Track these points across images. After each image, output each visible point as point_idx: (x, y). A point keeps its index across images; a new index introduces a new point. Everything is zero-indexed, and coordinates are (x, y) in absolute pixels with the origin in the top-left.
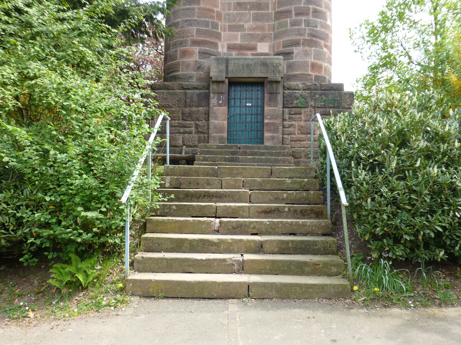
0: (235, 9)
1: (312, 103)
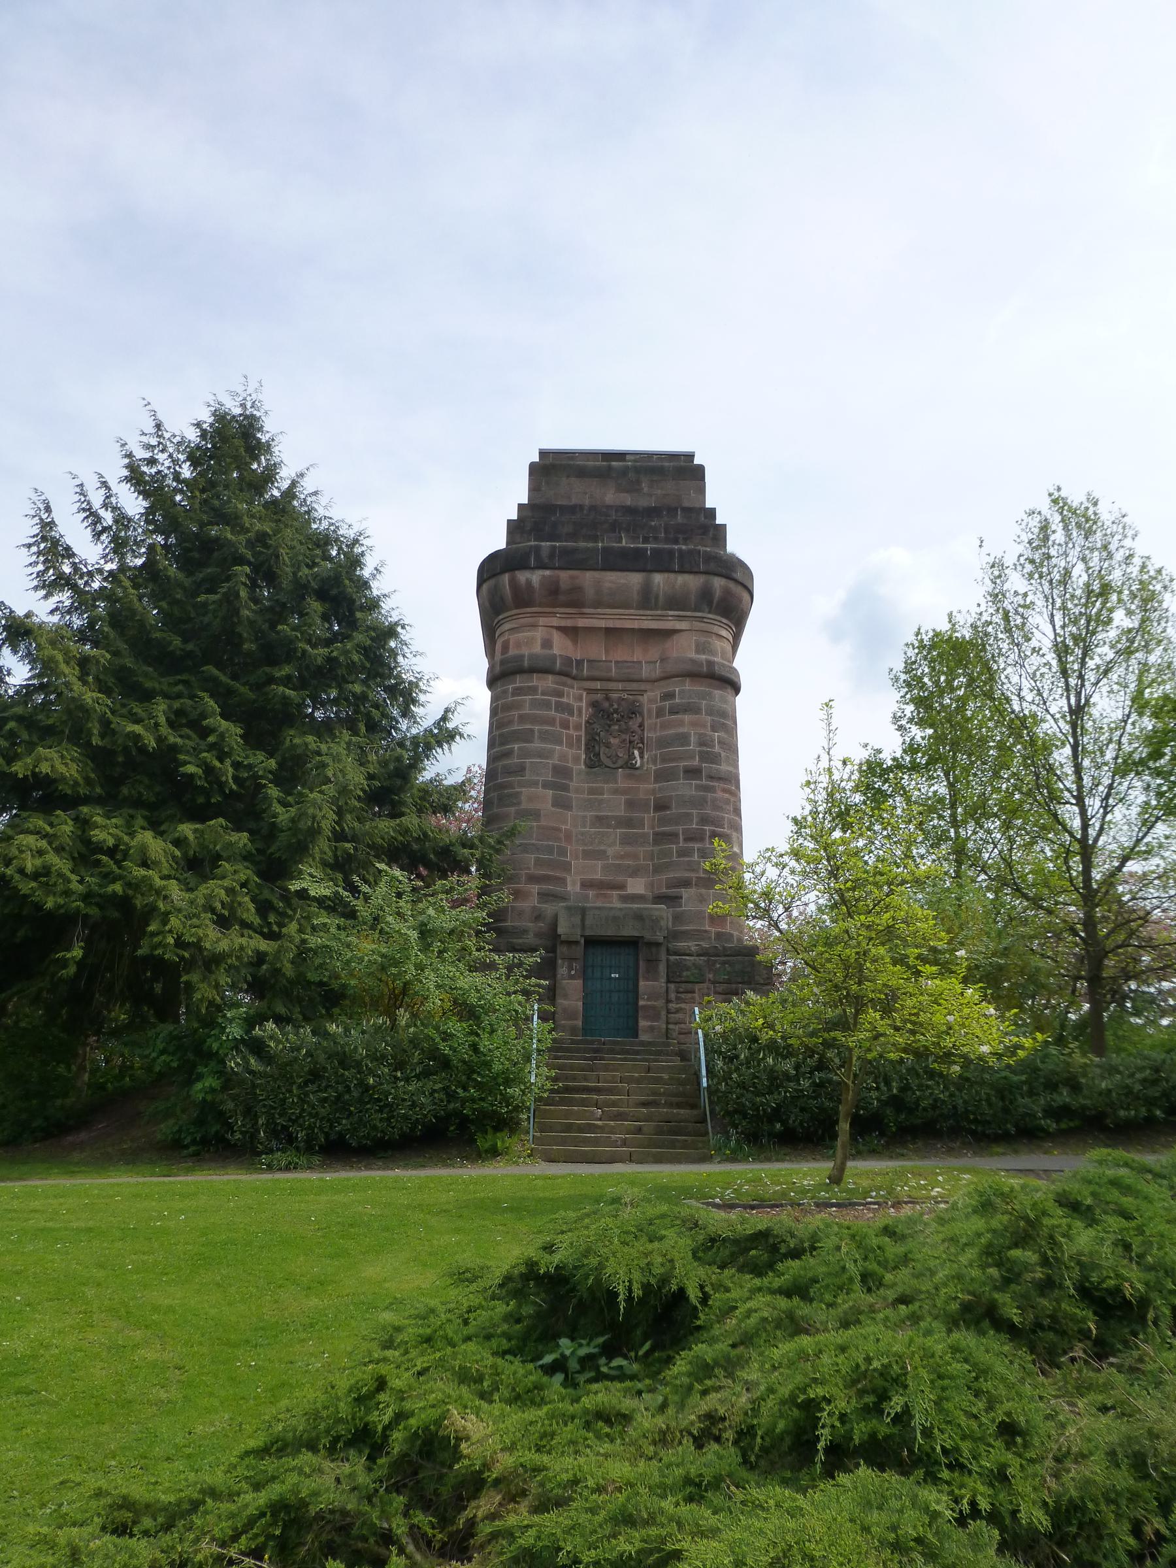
0: (593, 825)
1: (711, 976)
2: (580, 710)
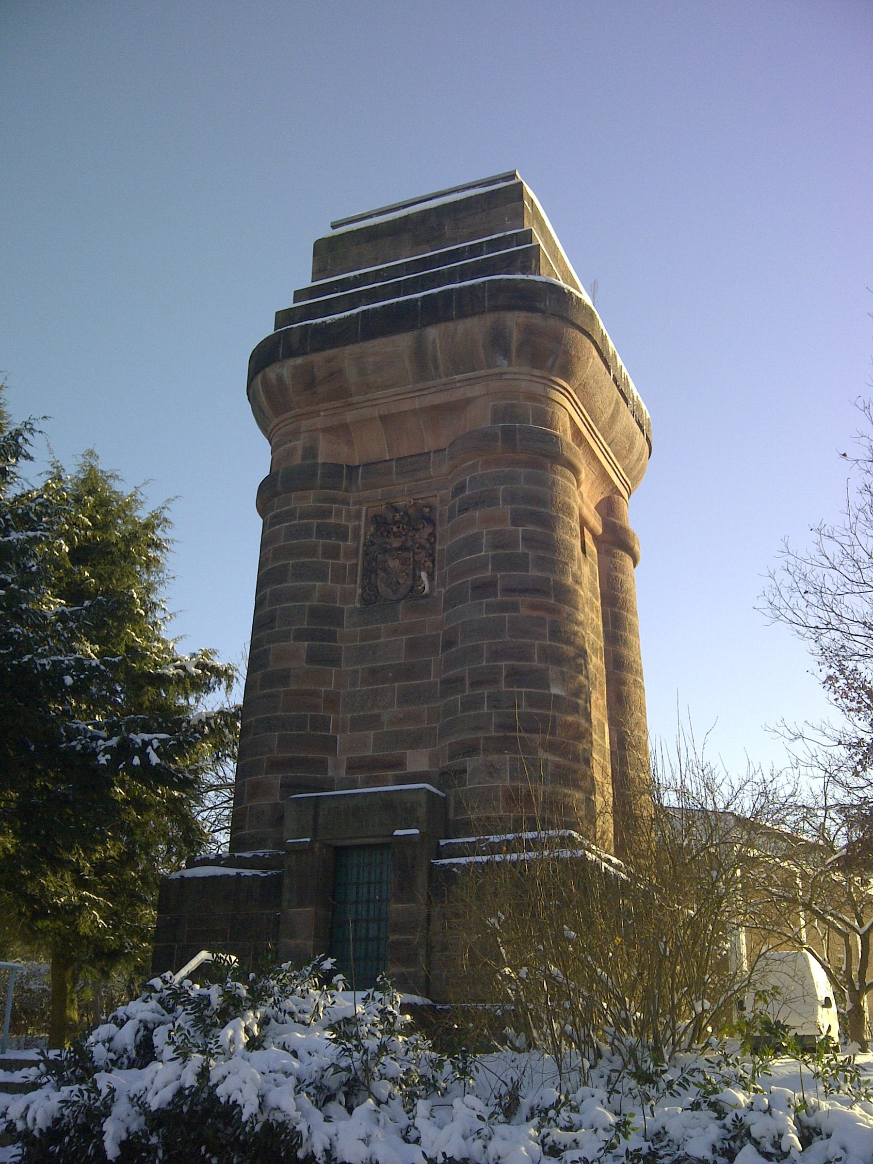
2: (357, 529)
